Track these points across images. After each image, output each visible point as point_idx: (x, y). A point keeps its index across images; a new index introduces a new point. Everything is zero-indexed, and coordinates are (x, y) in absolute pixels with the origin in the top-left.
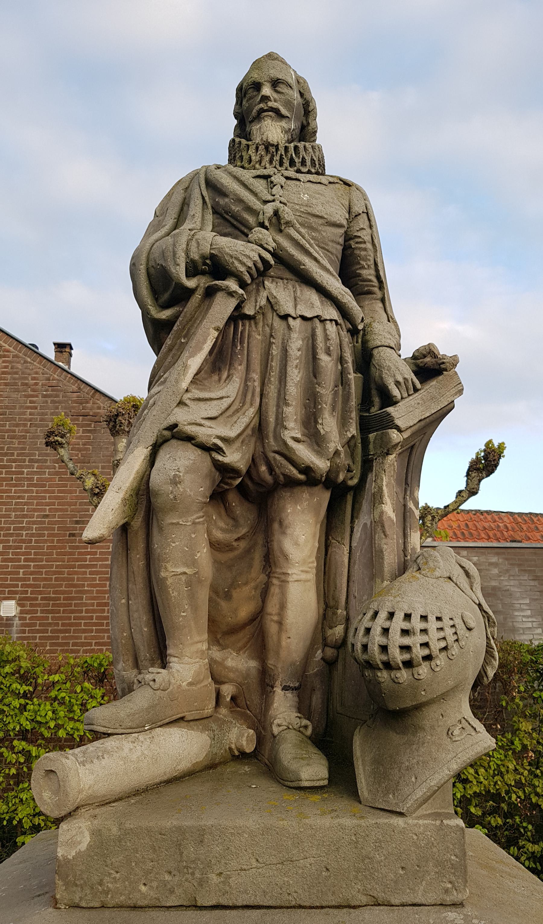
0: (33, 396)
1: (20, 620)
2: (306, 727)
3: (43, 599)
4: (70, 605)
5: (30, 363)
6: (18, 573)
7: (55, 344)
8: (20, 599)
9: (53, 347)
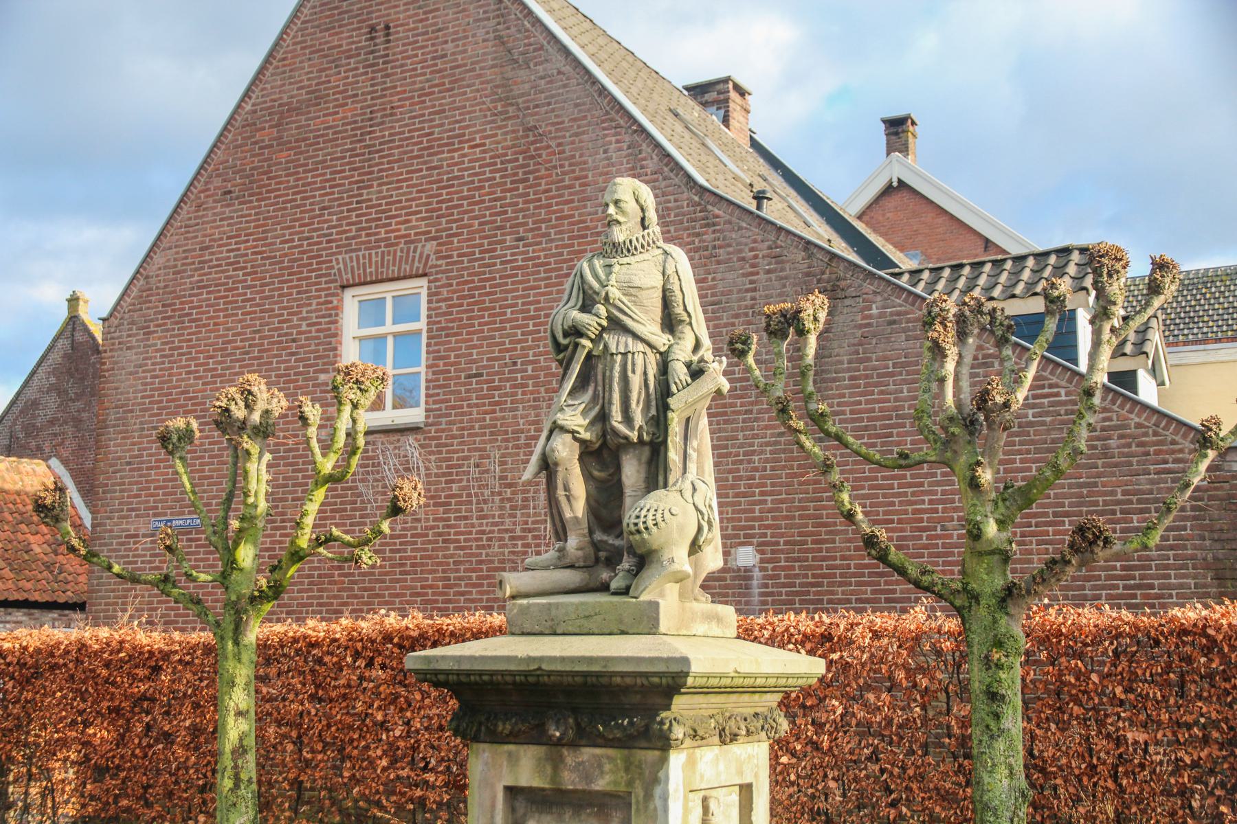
0: (752, 274)
4: (820, 550)
6: (753, 511)
7: (884, 121)
9: (883, 126)
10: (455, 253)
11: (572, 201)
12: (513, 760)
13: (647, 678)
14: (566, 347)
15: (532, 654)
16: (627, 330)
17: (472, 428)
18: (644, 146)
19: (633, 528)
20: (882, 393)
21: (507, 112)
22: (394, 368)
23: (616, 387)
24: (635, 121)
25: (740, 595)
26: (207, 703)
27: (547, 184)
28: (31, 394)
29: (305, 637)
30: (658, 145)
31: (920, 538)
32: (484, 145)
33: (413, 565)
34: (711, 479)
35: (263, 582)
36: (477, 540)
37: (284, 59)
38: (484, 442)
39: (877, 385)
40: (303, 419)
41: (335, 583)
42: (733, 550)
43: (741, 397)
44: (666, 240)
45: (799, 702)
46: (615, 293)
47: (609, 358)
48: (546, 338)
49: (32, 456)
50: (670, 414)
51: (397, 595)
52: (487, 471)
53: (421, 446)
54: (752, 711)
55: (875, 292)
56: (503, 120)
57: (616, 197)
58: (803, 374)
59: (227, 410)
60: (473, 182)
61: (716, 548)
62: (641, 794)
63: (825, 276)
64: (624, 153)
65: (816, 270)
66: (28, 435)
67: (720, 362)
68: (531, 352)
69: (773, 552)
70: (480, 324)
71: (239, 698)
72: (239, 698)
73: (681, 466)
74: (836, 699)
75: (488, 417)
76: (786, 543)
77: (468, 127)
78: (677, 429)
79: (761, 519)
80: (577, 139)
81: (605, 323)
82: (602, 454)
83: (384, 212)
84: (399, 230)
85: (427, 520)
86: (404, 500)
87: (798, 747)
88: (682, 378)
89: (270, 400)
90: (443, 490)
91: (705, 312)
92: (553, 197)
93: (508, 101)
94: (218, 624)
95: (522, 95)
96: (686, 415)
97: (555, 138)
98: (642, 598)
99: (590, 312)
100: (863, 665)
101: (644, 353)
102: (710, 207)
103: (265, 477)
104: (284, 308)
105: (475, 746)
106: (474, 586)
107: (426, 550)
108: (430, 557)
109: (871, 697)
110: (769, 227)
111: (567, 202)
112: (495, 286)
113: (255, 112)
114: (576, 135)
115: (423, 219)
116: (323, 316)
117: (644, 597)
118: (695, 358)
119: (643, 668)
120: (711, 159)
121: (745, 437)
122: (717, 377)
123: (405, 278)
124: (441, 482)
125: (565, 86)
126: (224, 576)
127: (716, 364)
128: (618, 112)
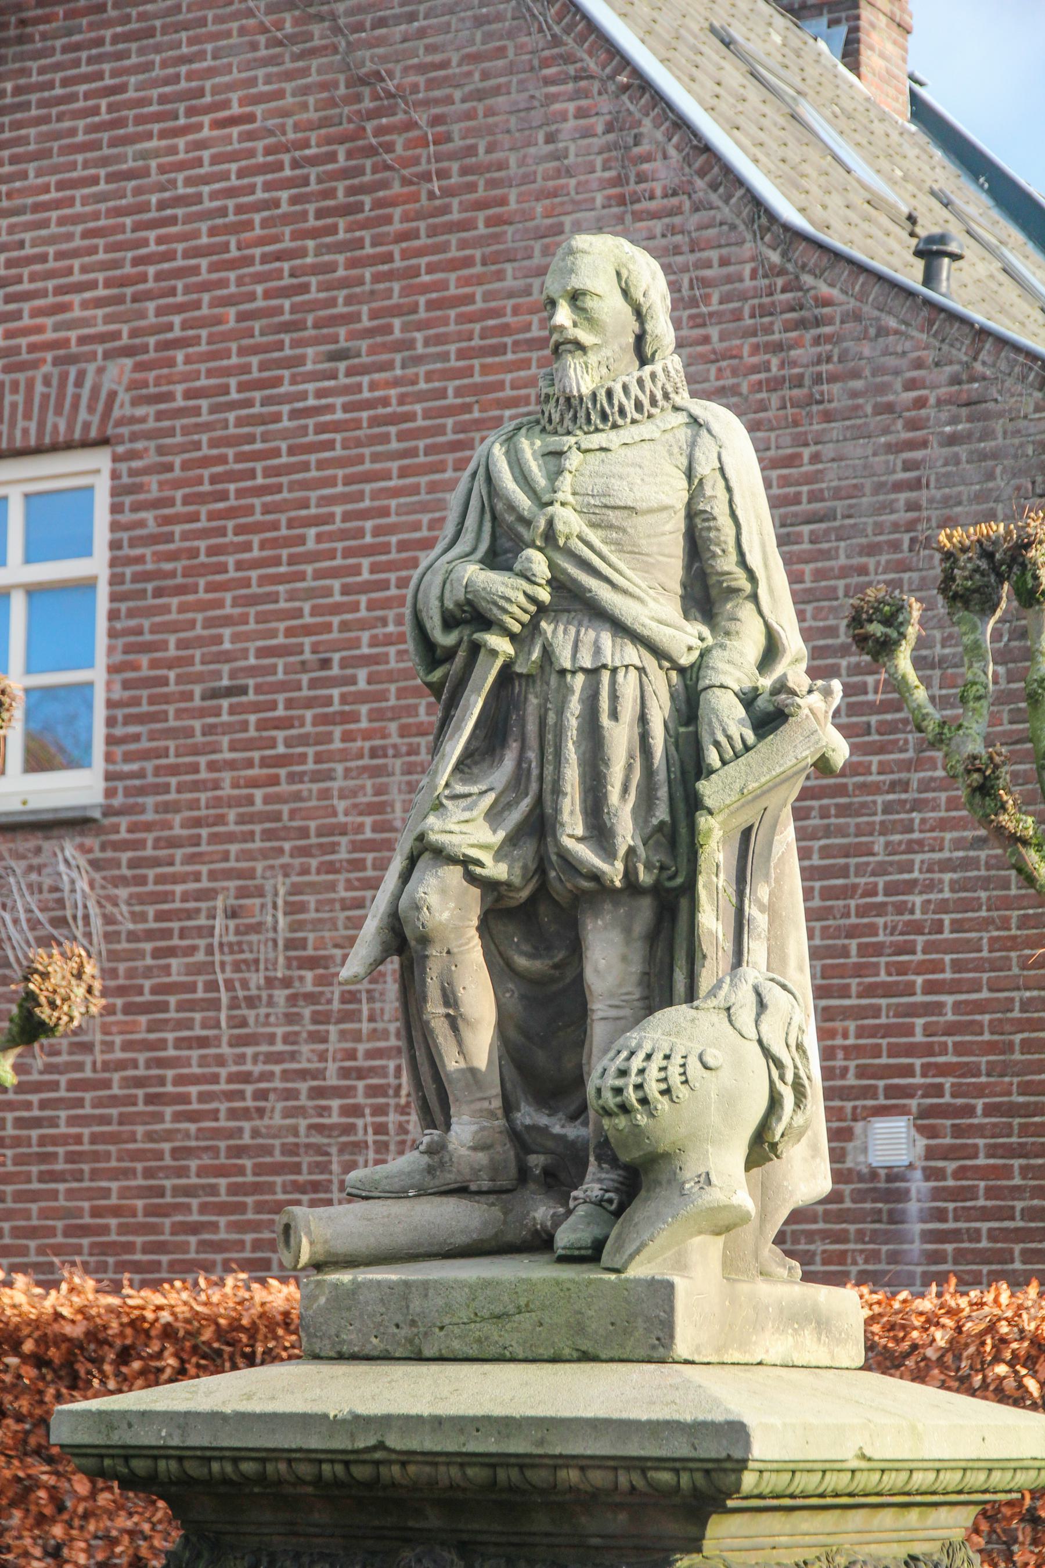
1: (927, 1179)
2: (610, 1201)
3: (990, 1110)
5: (897, 332)
6: (909, 1031)
8: (925, 1113)
10: (179, 389)
11: (467, 262)
13: (644, 1471)
14: (450, 654)
15: (362, 1410)
17: (221, 820)
18: (647, 122)
19: (610, 1100)
21: (309, 37)
22: (29, 670)
23: (571, 753)
24: (625, 62)
25: (875, 1237)
27: (406, 218)
30: (681, 124)
32: (250, 118)
33: (72, 1158)
34: (801, 975)
36: (230, 1096)
38: (246, 855)
42: (858, 1127)
43: (881, 749)
44: (693, 395)
46: (569, 521)
47: (554, 680)
48: (401, 638)
50: (704, 821)
51: (32, 1232)
52: (257, 928)
53: (95, 864)
56: (296, 58)
57: (575, 283)
60: (223, 212)
61: (814, 1148)
64: (597, 142)
67: (827, 693)
68: (365, 636)
70: (240, 566)
73: (729, 946)
75: (259, 794)
77: (211, 72)
78: (720, 857)
79: (928, 1050)
80: (480, 108)
81: (544, 595)
82: (537, 915)
84: (40, 329)
86: (53, 1005)
88: (734, 731)
90: (148, 972)
91: (794, 578)
92: (420, 253)
96: (742, 821)
97: (426, 103)
99: (509, 568)
101: (641, 670)
102: (807, 279)
106: (223, 1209)
107: (105, 1120)
108: (113, 1138)
111: (453, 265)
112: (277, 471)
114: (479, 95)
115: (99, 303)
117: (638, 1270)
118: (766, 683)
119: (633, 1449)
120: (813, 154)
121: (891, 849)
122: (820, 730)
123: (55, 448)
124: (140, 954)
127: (816, 699)
128: (581, 39)
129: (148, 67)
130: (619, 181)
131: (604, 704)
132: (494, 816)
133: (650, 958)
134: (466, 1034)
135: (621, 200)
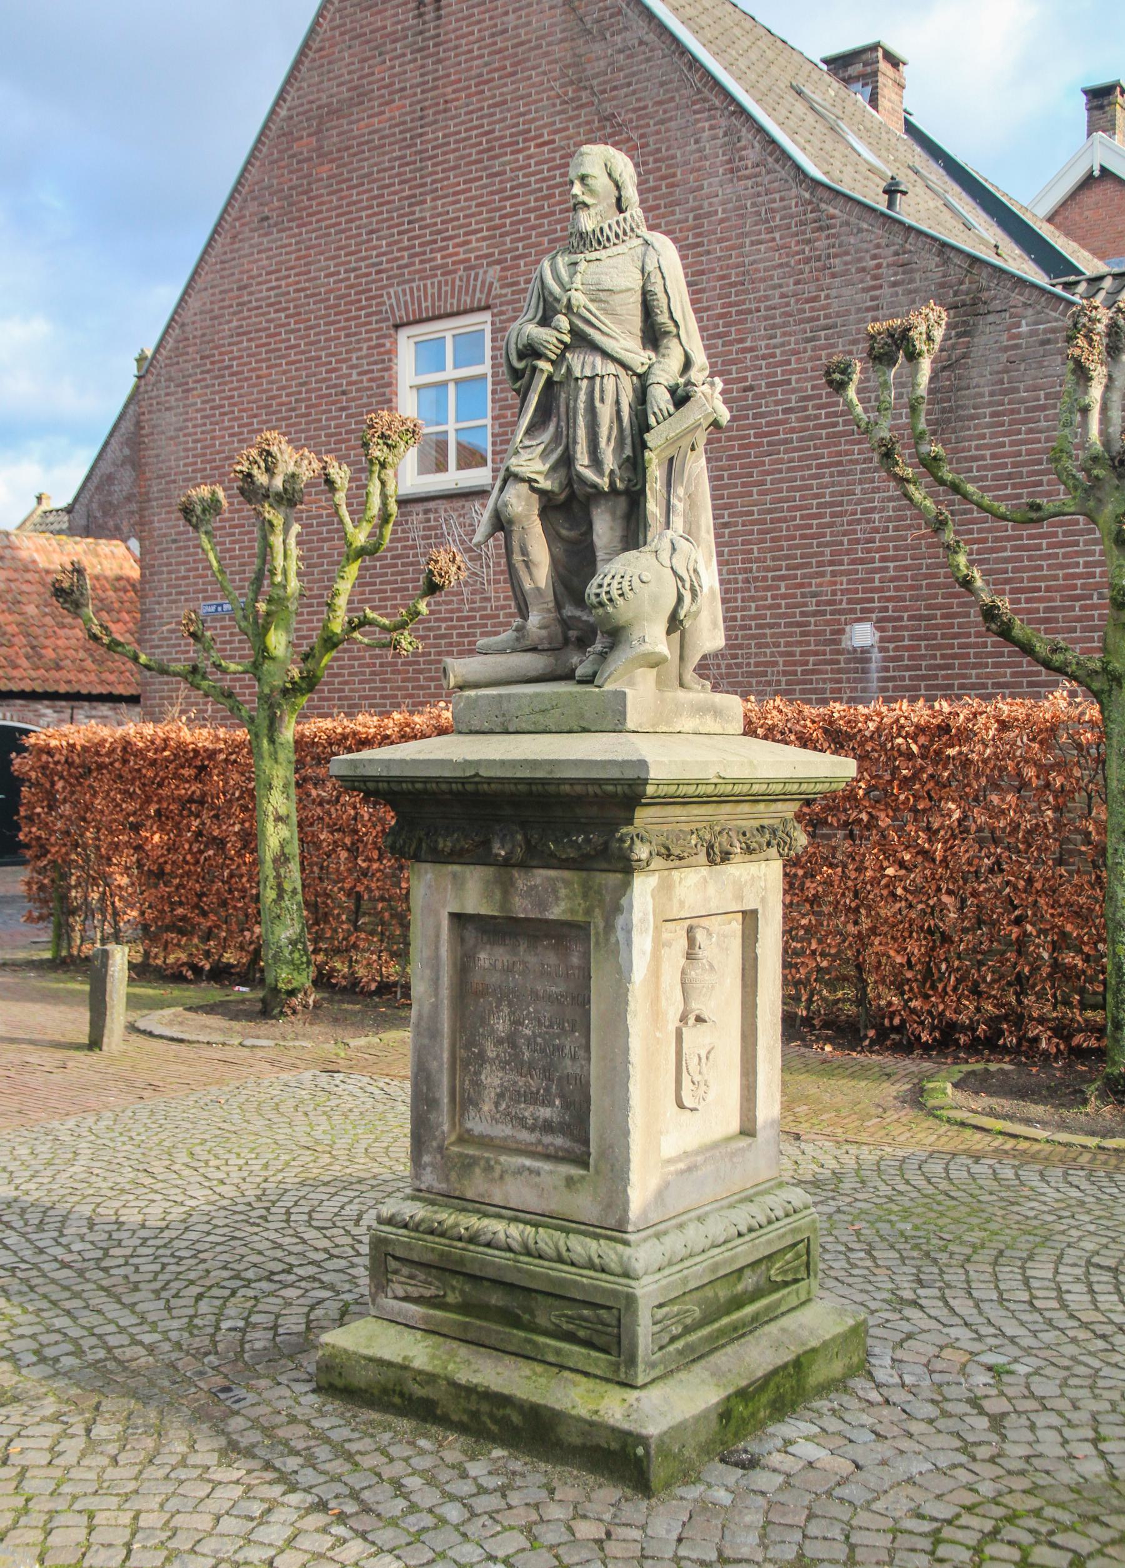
0: (874, 288)
6: (872, 581)
7: (1086, 92)
8: (880, 620)
12: (459, 883)
14: (524, 370)
16: (595, 348)
20: (1030, 431)
22: (457, 421)
23: (581, 422)
25: (855, 680)
26: (249, 802)
28: (105, 468)
29: (355, 733)
30: (761, 130)
31: (1072, 608)
32: (553, 142)
35: (295, 673)
37: (321, 49)
39: (1024, 422)
40: (329, 482)
41: (398, 672)
45: (820, 812)
46: (579, 299)
49: (113, 537)
50: (648, 454)
54: (756, 824)
55: (1025, 305)
57: (583, 171)
58: (913, 409)
59: (250, 475)
60: (541, 190)
62: (601, 925)
63: (963, 287)
65: (952, 279)
66: (105, 514)
69: (895, 629)
71: (278, 801)
72: (278, 801)
74: (953, 801)
76: (910, 618)
81: (567, 339)
83: (439, 232)
85: (498, 599)
87: (907, 857)
88: (663, 406)
89: (293, 462)
93: (580, 84)
94: (252, 719)
95: (597, 76)
96: (668, 454)
97: (637, 128)
98: (606, 688)
100: (985, 762)
102: (823, 206)
103: (294, 551)
104: (332, 355)
105: (418, 865)
109: (995, 799)
110: (896, 228)
113: (291, 118)
114: (662, 122)
115: (484, 239)
116: (376, 363)
117: (608, 687)
119: (594, 775)
122: (712, 400)
125: (648, 60)
126: (256, 666)
128: (711, 90)
129: (504, 120)
130: (730, 161)
131: (597, 395)
132: (544, 455)
133: (627, 527)
134: (534, 571)
135: (732, 171)
